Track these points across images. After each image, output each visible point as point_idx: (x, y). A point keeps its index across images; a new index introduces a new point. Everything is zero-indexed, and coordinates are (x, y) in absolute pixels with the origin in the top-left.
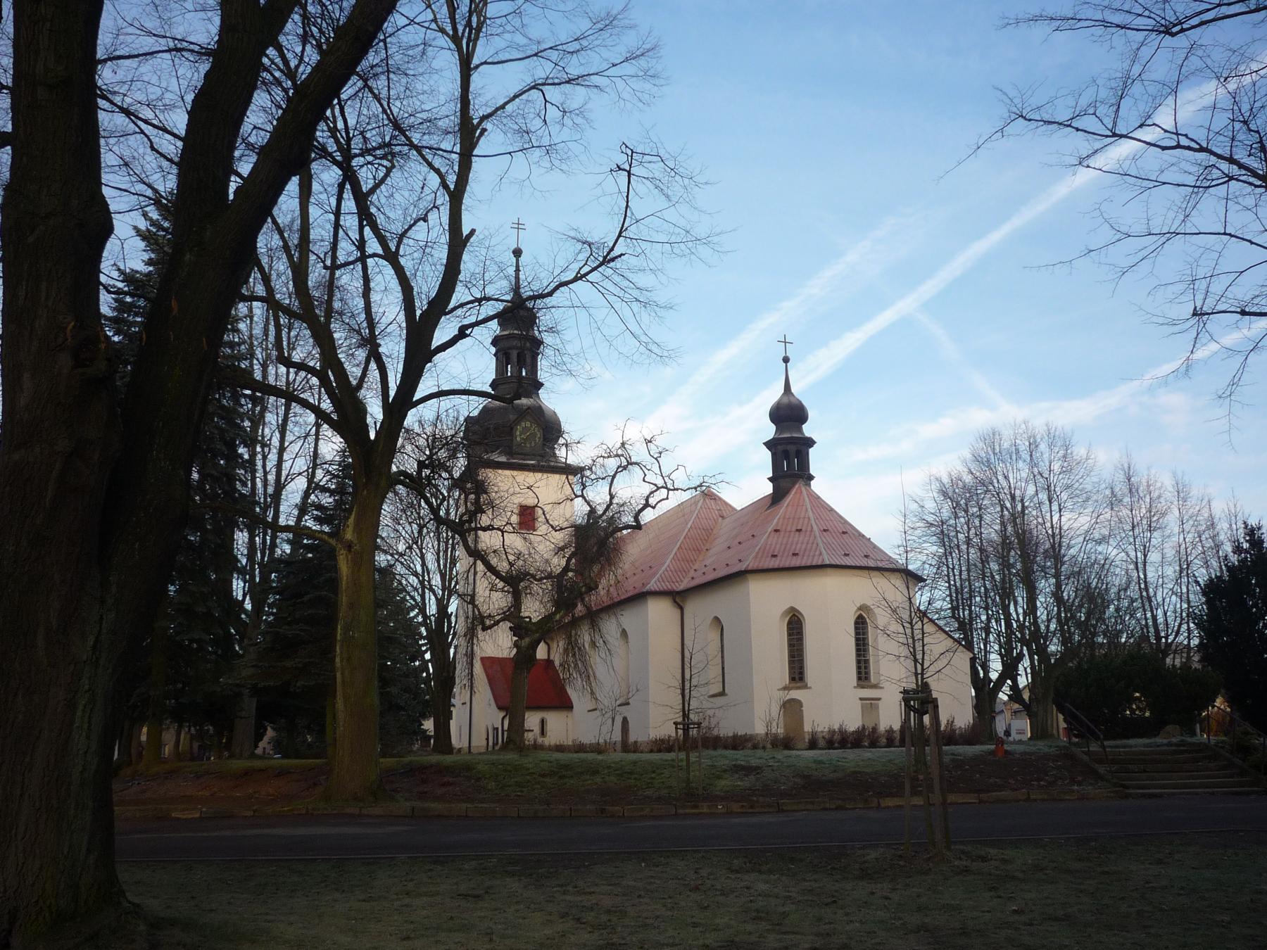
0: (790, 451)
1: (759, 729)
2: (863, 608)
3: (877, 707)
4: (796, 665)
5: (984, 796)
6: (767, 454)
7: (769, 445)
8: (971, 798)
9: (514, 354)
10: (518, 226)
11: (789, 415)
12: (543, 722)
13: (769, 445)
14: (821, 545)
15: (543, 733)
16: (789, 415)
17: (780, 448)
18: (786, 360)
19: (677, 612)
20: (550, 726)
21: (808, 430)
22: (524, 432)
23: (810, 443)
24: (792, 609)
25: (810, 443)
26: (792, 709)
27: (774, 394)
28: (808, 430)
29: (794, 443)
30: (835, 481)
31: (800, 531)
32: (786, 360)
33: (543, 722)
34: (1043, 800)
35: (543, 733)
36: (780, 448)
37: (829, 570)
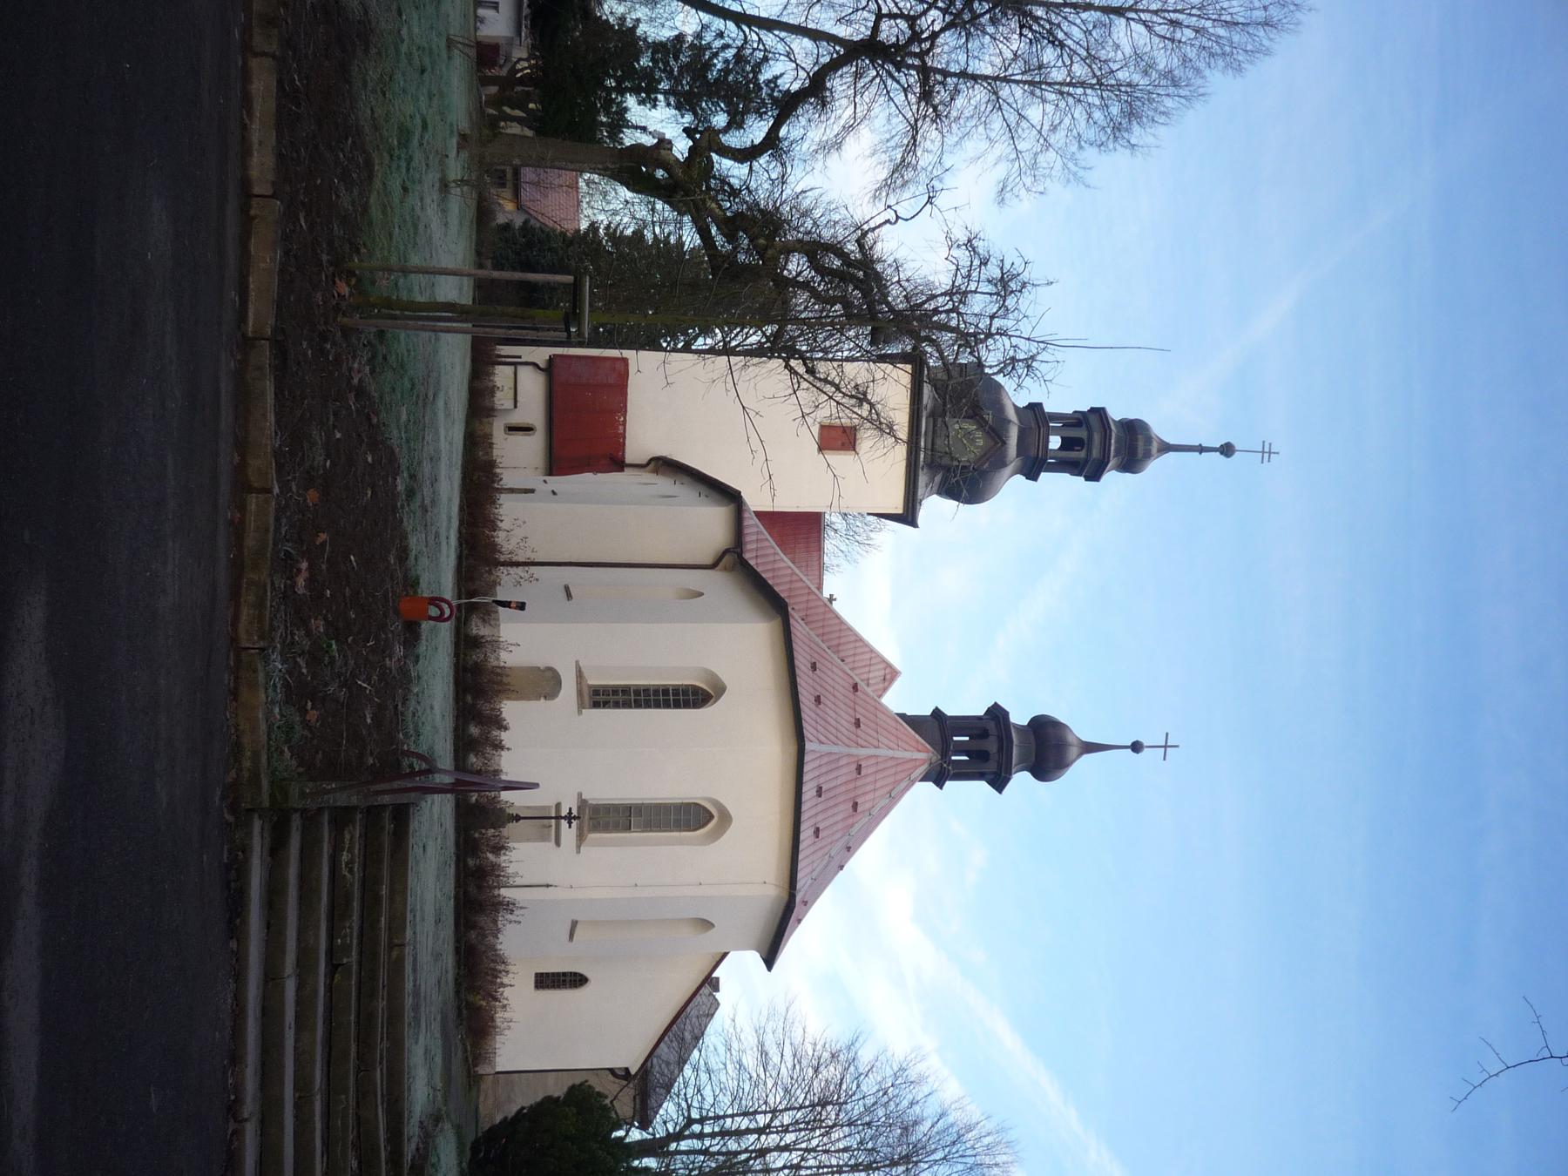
0: (990, 747)
1: (510, 765)
2: (726, 819)
3: (544, 838)
4: (620, 697)
5: (264, 355)
6: (976, 708)
7: (997, 714)
8: (260, 314)
9: (1081, 433)
10: (1267, 453)
11: (1046, 749)
12: (528, 429)
13: (997, 714)
14: (834, 749)
15: (512, 429)
16: (1046, 749)
17: (991, 726)
18: (1136, 747)
19: (709, 561)
20: (519, 438)
21: (1022, 781)
22: (966, 439)
23: (999, 783)
24: (720, 689)
25: (999, 783)
26: (545, 683)
27: (1081, 728)
28: (1022, 781)
29: (1000, 749)
30: (930, 832)
31: (857, 724)
32: (1136, 747)
33: (528, 429)
34: (238, 530)
35: (512, 429)
36: (991, 726)
37: (793, 749)
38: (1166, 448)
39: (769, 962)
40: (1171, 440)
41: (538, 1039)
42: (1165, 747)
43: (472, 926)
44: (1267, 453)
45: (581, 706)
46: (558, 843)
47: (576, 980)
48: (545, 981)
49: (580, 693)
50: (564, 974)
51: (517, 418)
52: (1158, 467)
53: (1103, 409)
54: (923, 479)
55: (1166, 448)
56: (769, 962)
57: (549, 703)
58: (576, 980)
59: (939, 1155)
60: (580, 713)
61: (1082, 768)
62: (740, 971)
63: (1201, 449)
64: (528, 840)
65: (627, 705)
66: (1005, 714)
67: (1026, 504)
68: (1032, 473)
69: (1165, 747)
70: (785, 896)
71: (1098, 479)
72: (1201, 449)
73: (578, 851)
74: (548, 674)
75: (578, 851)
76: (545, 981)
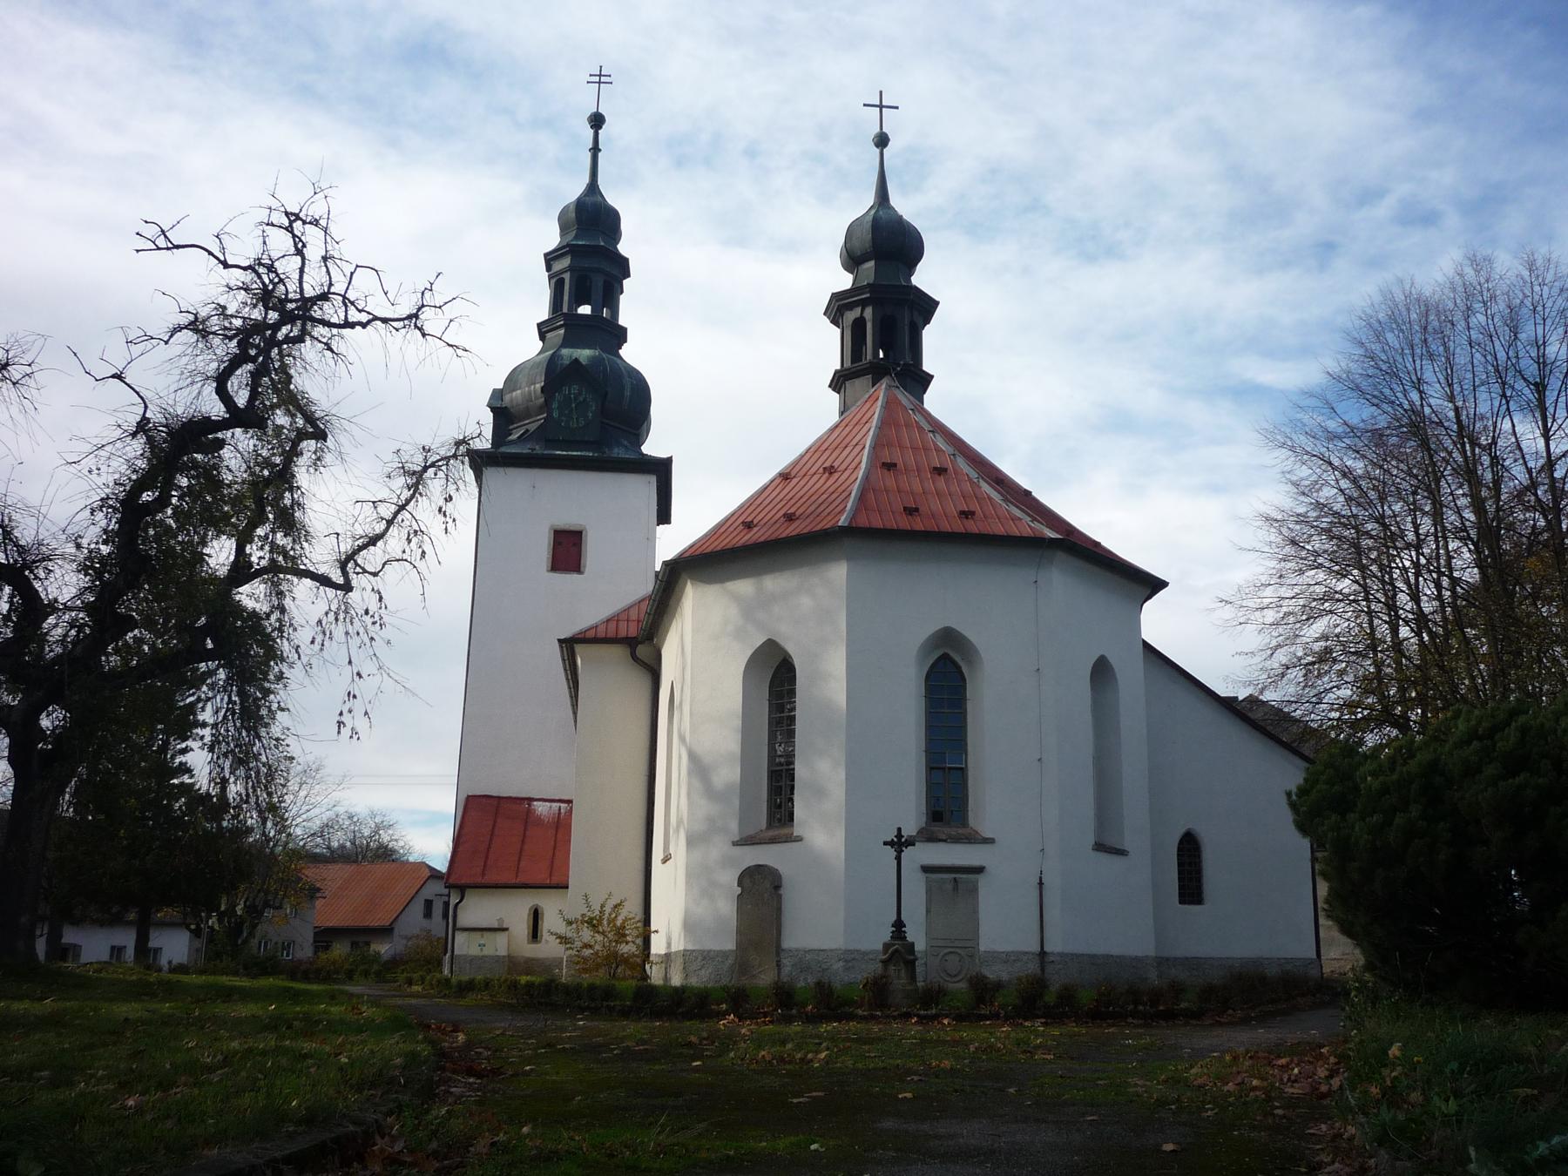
3: (974, 891)
7: (838, 307)
10: (600, 78)
12: (536, 915)
17: (851, 316)
21: (922, 278)
28: (922, 278)
33: (536, 915)
36: (851, 316)
38: (593, 187)
39: (1154, 585)
40: (586, 180)
41: (1273, 904)
42: (881, 107)
43: (1067, 995)
44: (600, 78)
45: (791, 839)
46: (979, 870)
47: (1189, 848)
48: (1191, 888)
49: (773, 841)
50: (1180, 865)
51: (521, 927)
52: (613, 197)
53: (546, 255)
54: (619, 453)
55: (593, 187)
56: (1154, 585)
57: (785, 882)
58: (1189, 848)
59: (1415, 396)
60: (799, 839)
61: (904, 205)
62: (1159, 623)
63: (595, 150)
64: (975, 911)
65: (1199, 872)
66: (836, 297)
67: (650, 340)
68: (620, 335)
69: (881, 107)
70: (1060, 556)
71: (626, 260)
72: (595, 150)
73: (990, 841)
74: (747, 881)
75: (990, 841)
76: (1191, 888)
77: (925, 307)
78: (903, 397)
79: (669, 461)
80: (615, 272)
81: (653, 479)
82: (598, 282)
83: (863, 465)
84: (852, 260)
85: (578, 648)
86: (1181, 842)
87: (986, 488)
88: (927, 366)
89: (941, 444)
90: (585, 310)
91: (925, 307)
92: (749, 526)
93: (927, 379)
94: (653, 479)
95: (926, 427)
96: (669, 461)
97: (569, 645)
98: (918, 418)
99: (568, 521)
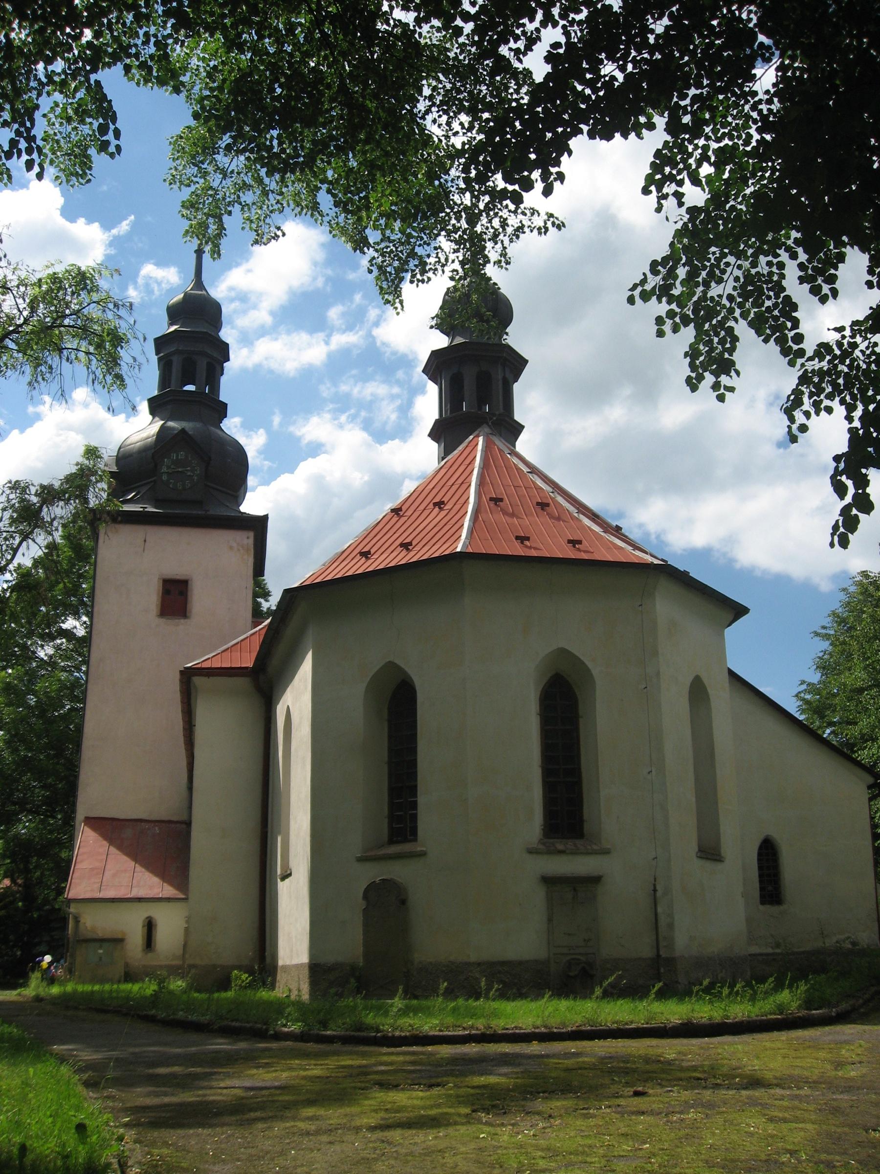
39: (739, 611)
47: (768, 852)
56: (739, 611)
58: (768, 852)
65: (413, 764)
68: (221, 410)
77: (516, 364)
78: (499, 443)
79: (265, 518)
80: (215, 354)
81: (251, 534)
82: (202, 365)
83: (472, 500)
84: (595, 138)
85: (197, 680)
86: (760, 848)
87: (587, 522)
88: (518, 417)
89: (540, 483)
90: (191, 388)
91: (516, 364)
92: (366, 555)
93: (518, 429)
94: (251, 534)
95: (525, 469)
96: (265, 518)
97: (188, 676)
98: (515, 460)
99: (175, 571)
